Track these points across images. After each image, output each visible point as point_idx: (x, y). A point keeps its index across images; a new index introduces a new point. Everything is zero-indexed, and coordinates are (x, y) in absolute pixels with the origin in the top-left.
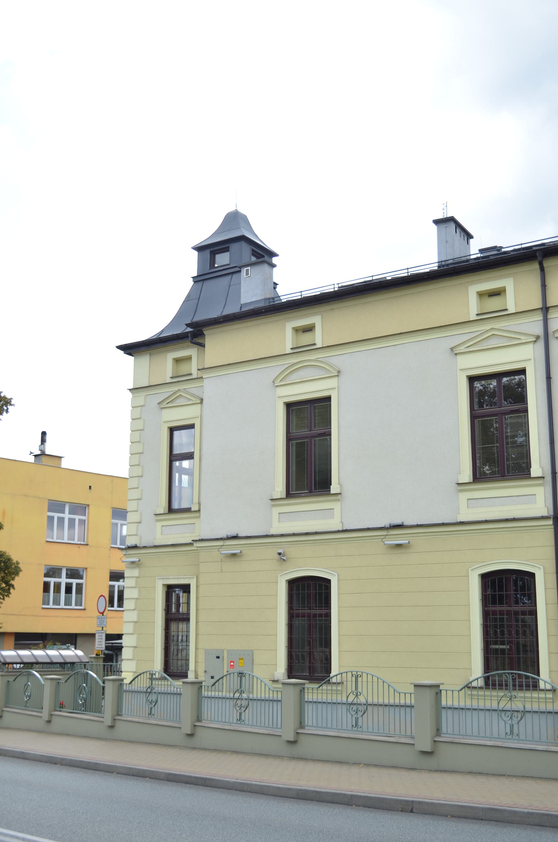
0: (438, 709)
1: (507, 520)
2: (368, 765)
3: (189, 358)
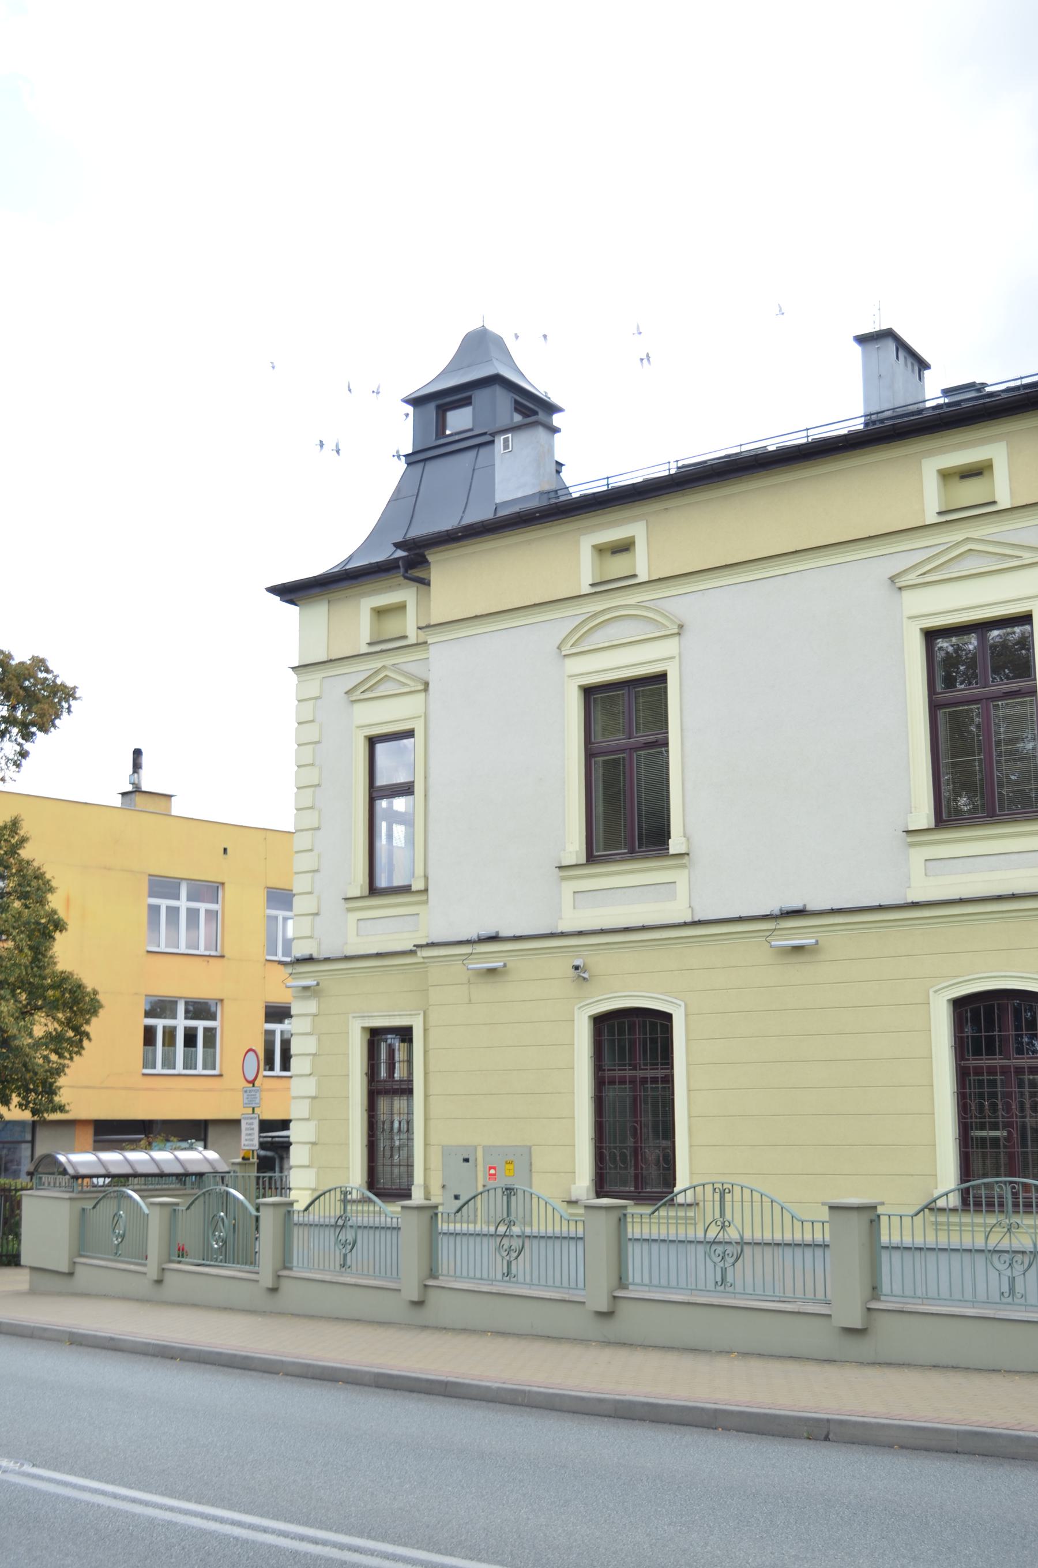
0: (875, 1250)
1: (1000, 898)
2: (745, 1355)
3: (401, 607)
